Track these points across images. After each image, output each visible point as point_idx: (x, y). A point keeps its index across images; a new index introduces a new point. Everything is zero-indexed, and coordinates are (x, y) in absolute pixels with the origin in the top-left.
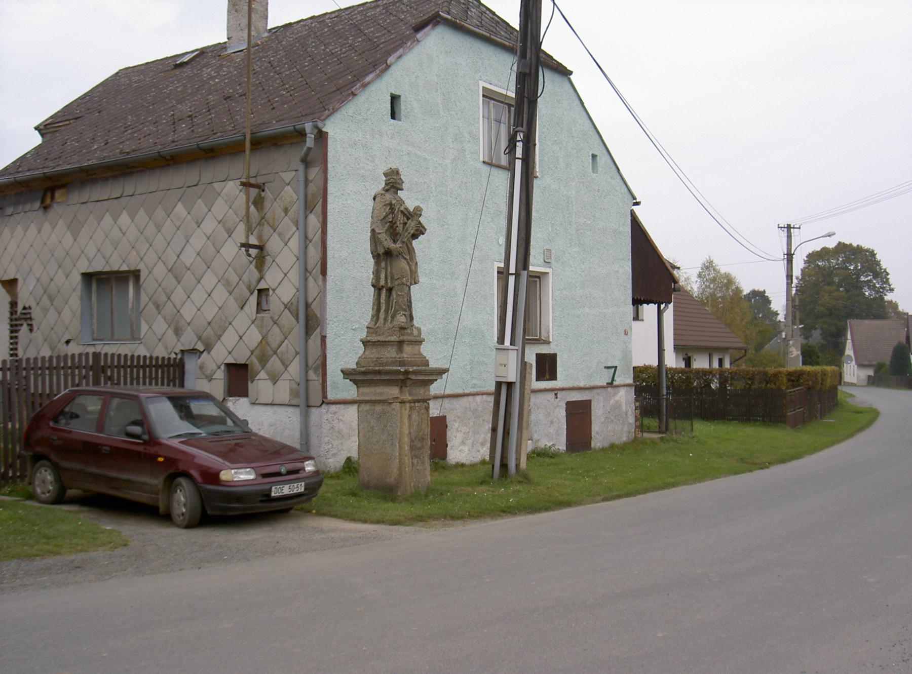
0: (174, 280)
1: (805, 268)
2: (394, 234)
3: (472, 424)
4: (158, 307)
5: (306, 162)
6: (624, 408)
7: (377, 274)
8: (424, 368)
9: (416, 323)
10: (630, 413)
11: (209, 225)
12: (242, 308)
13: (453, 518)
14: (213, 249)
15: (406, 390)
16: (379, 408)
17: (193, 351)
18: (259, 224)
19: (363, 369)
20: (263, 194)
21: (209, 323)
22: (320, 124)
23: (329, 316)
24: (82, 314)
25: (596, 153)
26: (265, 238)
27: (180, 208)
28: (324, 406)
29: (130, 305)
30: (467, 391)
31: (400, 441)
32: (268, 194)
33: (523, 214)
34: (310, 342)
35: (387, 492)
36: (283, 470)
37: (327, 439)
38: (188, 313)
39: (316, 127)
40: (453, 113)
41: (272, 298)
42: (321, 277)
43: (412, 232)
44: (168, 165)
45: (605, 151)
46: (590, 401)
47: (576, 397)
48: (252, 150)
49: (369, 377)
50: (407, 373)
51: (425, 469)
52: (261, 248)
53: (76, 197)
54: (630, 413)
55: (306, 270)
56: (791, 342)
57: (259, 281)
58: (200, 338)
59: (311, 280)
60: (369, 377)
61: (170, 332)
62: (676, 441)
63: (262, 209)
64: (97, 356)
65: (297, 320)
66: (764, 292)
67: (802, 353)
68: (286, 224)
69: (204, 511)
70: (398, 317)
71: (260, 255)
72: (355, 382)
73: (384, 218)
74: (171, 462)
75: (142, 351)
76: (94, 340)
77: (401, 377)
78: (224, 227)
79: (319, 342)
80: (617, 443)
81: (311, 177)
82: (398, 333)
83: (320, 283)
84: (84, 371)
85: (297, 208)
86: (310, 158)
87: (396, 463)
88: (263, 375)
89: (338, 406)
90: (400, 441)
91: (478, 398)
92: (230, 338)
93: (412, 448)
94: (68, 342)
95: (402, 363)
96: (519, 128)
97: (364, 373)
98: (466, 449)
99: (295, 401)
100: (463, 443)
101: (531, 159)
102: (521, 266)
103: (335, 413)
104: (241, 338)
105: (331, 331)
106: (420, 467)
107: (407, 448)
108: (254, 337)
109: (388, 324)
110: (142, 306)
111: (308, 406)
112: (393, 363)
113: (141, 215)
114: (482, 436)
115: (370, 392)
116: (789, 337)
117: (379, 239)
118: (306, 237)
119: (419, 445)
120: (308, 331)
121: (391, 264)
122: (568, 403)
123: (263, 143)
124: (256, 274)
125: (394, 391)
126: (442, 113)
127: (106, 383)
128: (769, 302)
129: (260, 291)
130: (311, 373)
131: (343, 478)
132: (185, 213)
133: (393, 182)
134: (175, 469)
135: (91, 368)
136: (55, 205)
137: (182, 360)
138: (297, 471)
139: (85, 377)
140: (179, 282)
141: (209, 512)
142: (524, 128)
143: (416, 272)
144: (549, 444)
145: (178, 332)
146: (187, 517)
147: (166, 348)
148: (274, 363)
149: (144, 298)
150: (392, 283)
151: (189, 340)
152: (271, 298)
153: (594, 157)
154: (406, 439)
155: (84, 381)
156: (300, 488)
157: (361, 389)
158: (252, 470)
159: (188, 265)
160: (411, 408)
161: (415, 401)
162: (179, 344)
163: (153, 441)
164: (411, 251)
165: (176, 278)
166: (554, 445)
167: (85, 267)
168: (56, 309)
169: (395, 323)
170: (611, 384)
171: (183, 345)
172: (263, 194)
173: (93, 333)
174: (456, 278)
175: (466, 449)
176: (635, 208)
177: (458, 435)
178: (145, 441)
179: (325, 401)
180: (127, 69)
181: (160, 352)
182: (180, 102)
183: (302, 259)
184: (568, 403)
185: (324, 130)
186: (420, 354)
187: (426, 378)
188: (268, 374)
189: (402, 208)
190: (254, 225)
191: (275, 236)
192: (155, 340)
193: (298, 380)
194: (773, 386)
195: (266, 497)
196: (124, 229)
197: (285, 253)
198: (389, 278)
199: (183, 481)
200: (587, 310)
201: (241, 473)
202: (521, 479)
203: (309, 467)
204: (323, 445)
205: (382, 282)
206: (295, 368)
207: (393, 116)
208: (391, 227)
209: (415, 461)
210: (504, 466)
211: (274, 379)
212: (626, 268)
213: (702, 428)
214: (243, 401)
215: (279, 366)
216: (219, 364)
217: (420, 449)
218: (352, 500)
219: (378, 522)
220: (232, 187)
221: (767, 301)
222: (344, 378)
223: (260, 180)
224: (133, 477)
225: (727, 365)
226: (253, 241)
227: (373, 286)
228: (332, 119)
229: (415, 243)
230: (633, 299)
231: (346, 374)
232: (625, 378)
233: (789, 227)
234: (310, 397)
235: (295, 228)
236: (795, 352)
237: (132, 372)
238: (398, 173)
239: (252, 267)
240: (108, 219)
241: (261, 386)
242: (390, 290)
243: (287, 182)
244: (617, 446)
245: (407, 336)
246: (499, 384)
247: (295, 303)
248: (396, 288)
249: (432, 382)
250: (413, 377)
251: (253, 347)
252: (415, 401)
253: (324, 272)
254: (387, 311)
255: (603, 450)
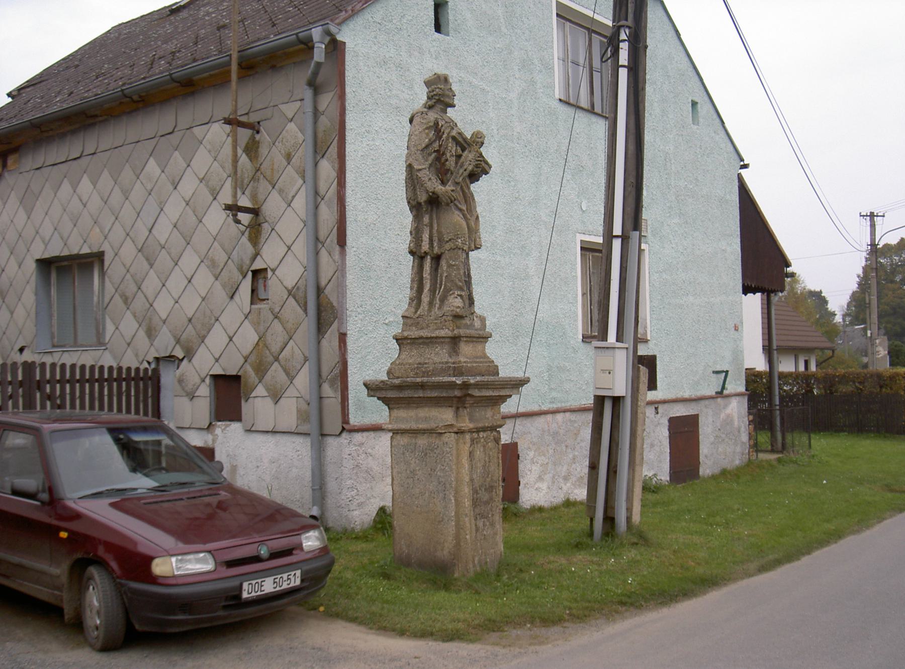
0: (145, 263)
1: (866, 265)
2: (443, 174)
3: (551, 451)
4: (126, 301)
5: (316, 87)
6: (736, 423)
7: (416, 234)
8: (492, 378)
9: (478, 309)
10: (743, 429)
11: (189, 186)
12: (232, 297)
13: (548, 621)
14: (194, 218)
15: (464, 413)
16: (422, 441)
17: (171, 358)
18: (253, 179)
19: (397, 381)
20: (258, 137)
21: (190, 320)
22: (333, 29)
23: (350, 304)
24: (37, 313)
25: (696, 100)
26: (261, 197)
27: (152, 166)
28: (344, 435)
29: (95, 299)
30: (545, 408)
31: (457, 492)
32: (264, 137)
33: (632, 147)
34: (324, 342)
35: (438, 573)
36: (264, 552)
37: (349, 482)
38: (163, 307)
39: (328, 33)
40: (519, 31)
41: (272, 282)
42: (337, 248)
43: (470, 168)
44: (136, 110)
45: (706, 98)
46: (698, 415)
47: (680, 411)
48: (241, 78)
49: (407, 394)
50: (466, 386)
51: (496, 534)
52: (255, 212)
53: (29, 161)
54: (743, 429)
55: (317, 239)
56: (877, 341)
57: (254, 259)
58: (178, 341)
59: (323, 253)
60: (407, 394)
61: (142, 333)
62: (795, 462)
63: (256, 157)
64: (29, 367)
65: (305, 311)
66: (821, 292)
67: (889, 353)
68: (290, 177)
69: (129, 625)
70: (451, 299)
71: (255, 222)
72: (386, 401)
73: (427, 147)
74: (78, 540)
75: (108, 360)
76: (54, 346)
77: (457, 393)
78: (207, 186)
79: (336, 343)
80: (729, 467)
81: (322, 107)
82: (451, 325)
83: (337, 256)
84: (10, 389)
85: (304, 154)
86: (320, 79)
87: (451, 528)
88: (260, 390)
89: (365, 434)
90: (457, 492)
91: (559, 417)
92: (216, 339)
93: (475, 503)
94: (21, 350)
95: (458, 371)
96: (623, 23)
97: (400, 387)
98: (544, 486)
99: (304, 428)
100: (540, 479)
101: (641, 68)
102: (629, 225)
103: (361, 444)
104: (231, 339)
105: (352, 329)
106: (488, 532)
107: (467, 503)
108: (248, 337)
109: (436, 311)
110: (107, 300)
111: (323, 435)
112: (444, 371)
113: (106, 179)
114: (565, 468)
115: (410, 417)
116: (875, 336)
117: (418, 178)
118: (316, 193)
119: (485, 496)
120: (321, 327)
121: (438, 219)
122: (671, 420)
123: (256, 65)
124: (250, 249)
125: (446, 415)
126: (504, 30)
127: (43, 407)
128: (826, 302)
129: (255, 273)
130: (326, 388)
131: (372, 540)
132: (158, 171)
133: (440, 95)
134: (89, 550)
135: (21, 384)
136: (6, 174)
137: (156, 371)
138: (288, 552)
139: (11, 397)
140: (151, 265)
141: (137, 627)
142: (630, 22)
143: (477, 231)
144: (650, 474)
145: (151, 333)
146: (102, 630)
147: (137, 355)
148: (276, 372)
149: (109, 288)
150: (440, 248)
151: (164, 344)
152: (270, 283)
153: (694, 104)
154: (466, 490)
155: (10, 402)
156: (293, 579)
157: (396, 413)
158: (208, 556)
159: (163, 242)
160: (472, 440)
161: (478, 430)
162: (152, 349)
163: (53, 500)
164: (468, 199)
165: (147, 260)
166: (655, 475)
167: (39, 251)
168: (8, 307)
169: (446, 308)
170: (720, 394)
171: (157, 351)
172: (258, 137)
173: (52, 337)
174: (528, 255)
175: (544, 486)
176: (743, 171)
177: (534, 468)
178: (43, 503)
179: (346, 428)
180: (120, 25)
181: (130, 361)
182: (165, 42)
183: (310, 224)
184: (671, 420)
185: (339, 38)
186: (485, 356)
187: (496, 393)
188: (267, 390)
189: (454, 133)
190: (246, 181)
191: (275, 193)
192: (124, 345)
193: (308, 397)
194: (889, 391)
195: (234, 599)
196: (85, 200)
197: (288, 219)
198: (435, 239)
199: (93, 571)
200: (691, 298)
201: (189, 561)
202: (635, 540)
203: (311, 541)
204: (344, 491)
205: (425, 247)
206: (303, 380)
207: (438, 28)
208: (438, 159)
209: (480, 523)
210: (609, 520)
211: (276, 396)
212: (734, 247)
213: (823, 446)
214: (236, 426)
215: (282, 377)
216: (203, 376)
217: (487, 503)
218: (383, 586)
219: (423, 634)
220: (218, 132)
221: (824, 301)
222: (369, 395)
223: (253, 118)
224: (26, 561)
225: (813, 368)
226: (244, 202)
227: (412, 253)
228: (351, 24)
229: (475, 187)
230: (743, 286)
231: (373, 388)
232: (737, 385)
233: (872, 216)
234: (325, 423)
235: (300, 181)
236: (882, 352)
237: (119, 387)
238: (446, 80)
239: (245, 240)
240: (66, 187)
241: (258, 406)
242: (437, 259)
243: (290, 117)
244: (729, 472)
245: (464, 330)
246: (600, 400)
247: (303, 288)
248: (447, 255)
249: (503, 399)
250: (476, 393)
251: (246, 352)
252: (478, 430)
253: (342, 241)
254: (433, 291)
255: (713, 477)
